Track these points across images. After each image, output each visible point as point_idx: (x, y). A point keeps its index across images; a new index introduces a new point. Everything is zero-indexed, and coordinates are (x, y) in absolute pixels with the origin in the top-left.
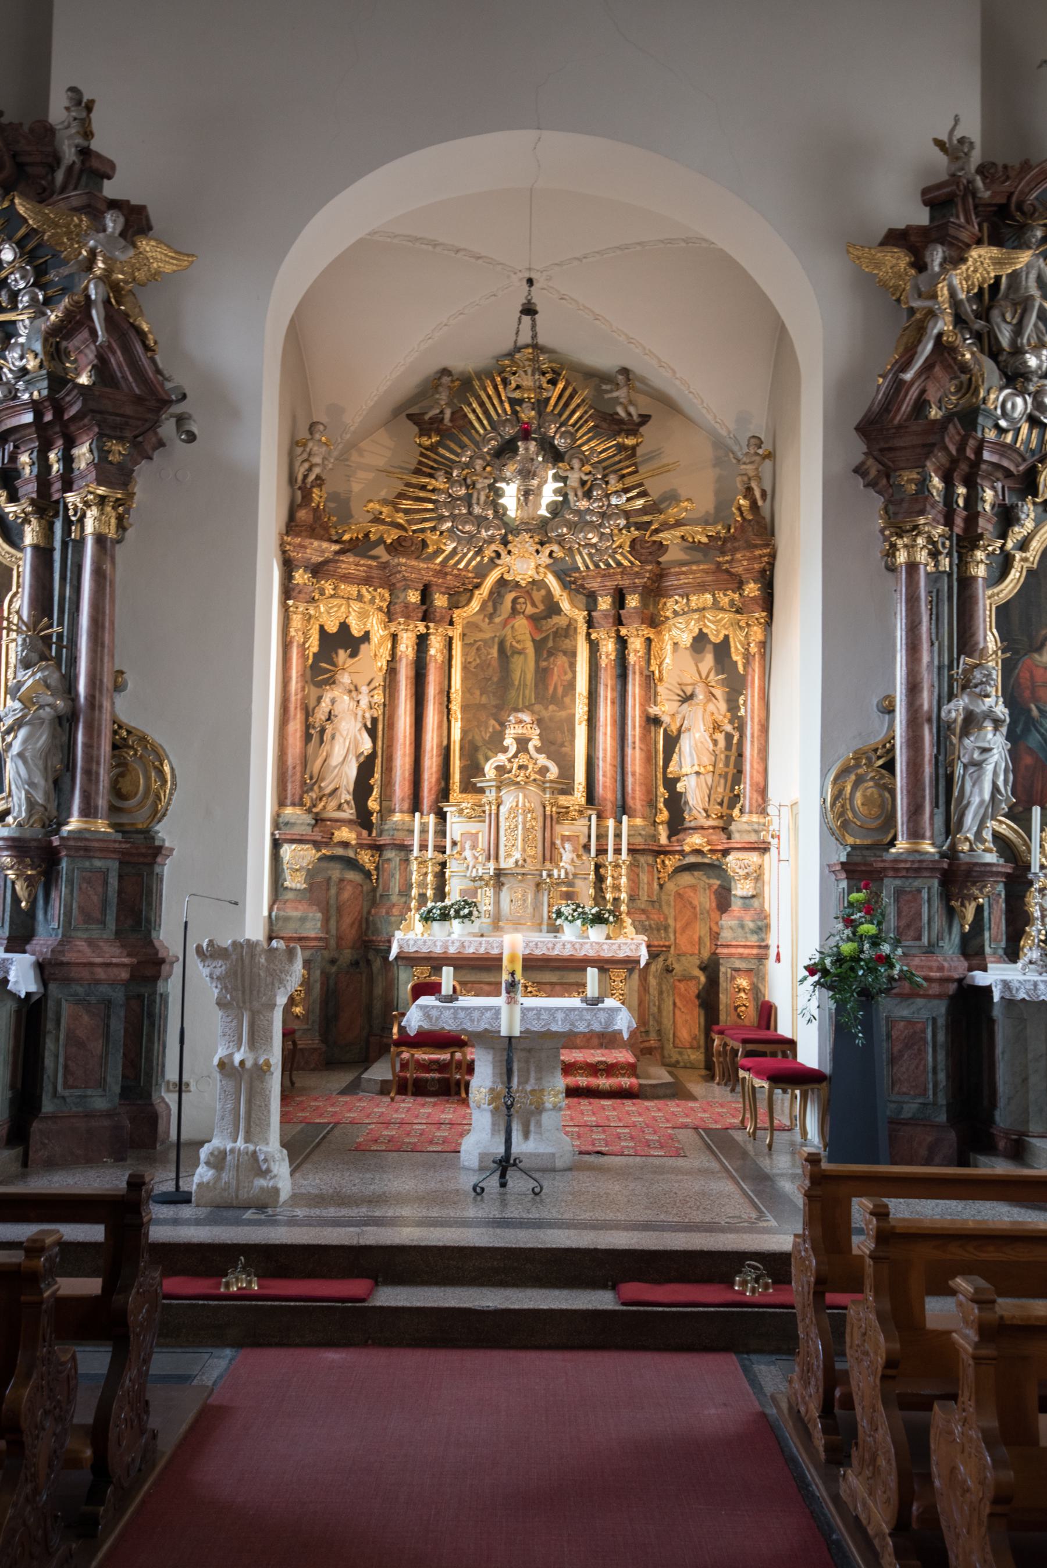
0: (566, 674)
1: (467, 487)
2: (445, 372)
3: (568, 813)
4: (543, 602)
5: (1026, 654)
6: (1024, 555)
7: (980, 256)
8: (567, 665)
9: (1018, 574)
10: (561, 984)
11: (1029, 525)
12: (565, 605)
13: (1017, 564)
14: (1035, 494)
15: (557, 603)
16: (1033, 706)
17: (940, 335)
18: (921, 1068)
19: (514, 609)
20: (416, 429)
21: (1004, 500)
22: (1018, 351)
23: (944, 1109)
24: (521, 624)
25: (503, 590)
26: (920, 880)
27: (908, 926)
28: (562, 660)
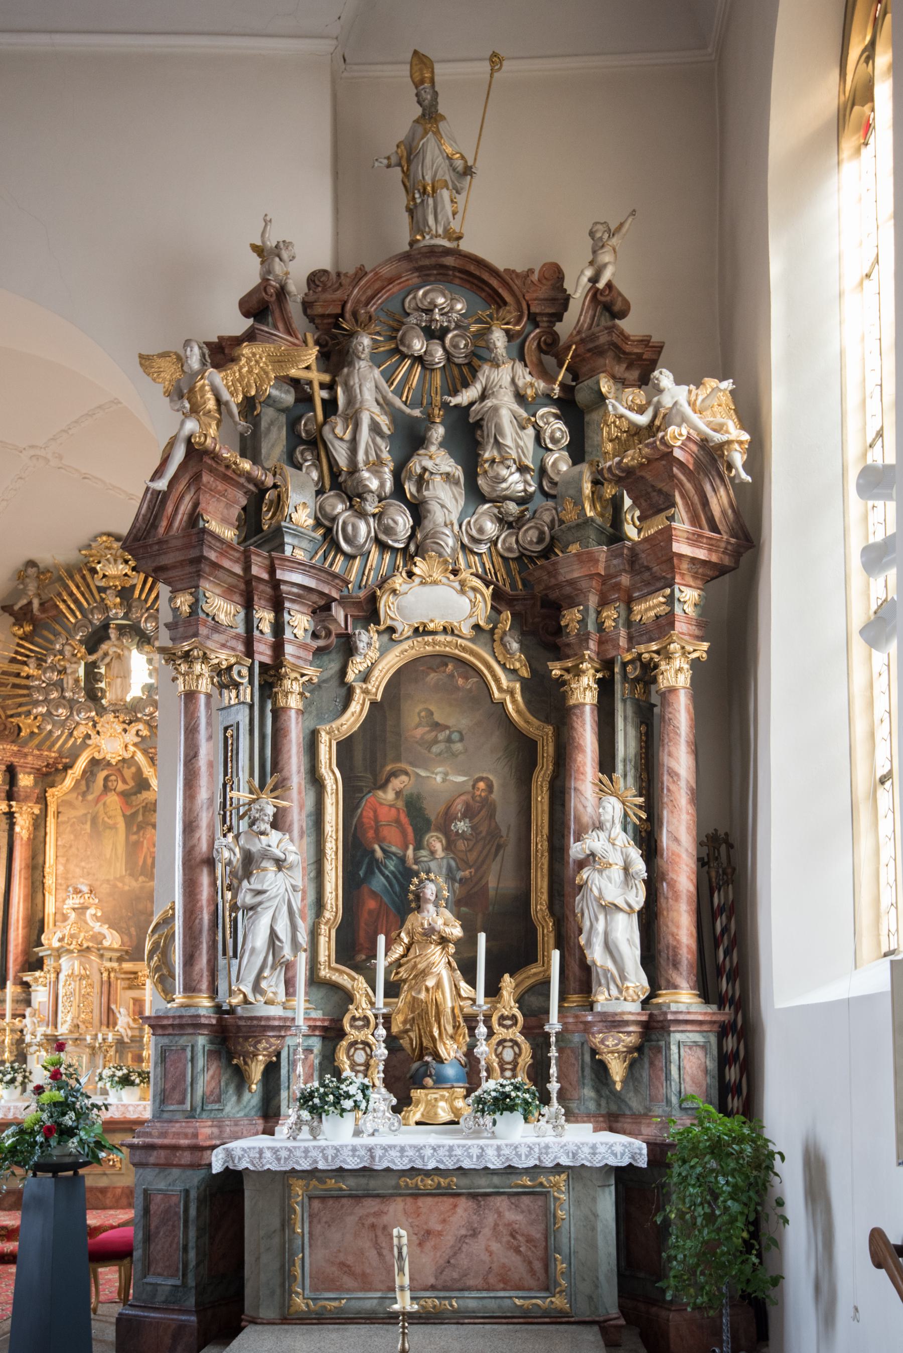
1: (60, 672)
2: (31, 563)
4: (133, 779)
5: (369, 792)
7: (254, 355)
11: (373, 654)
13: (358, 695)
14: (377, 623)
16: (377, 847)
18: (174, 1246)
19: (105, 786)
20: (12, 620)
21: (346, 628)
22: (354, 469)
23: (193, 1291)
24: (113, 799)
25: (95, 769)
26: (185, 1038)
27: (174, 1088)
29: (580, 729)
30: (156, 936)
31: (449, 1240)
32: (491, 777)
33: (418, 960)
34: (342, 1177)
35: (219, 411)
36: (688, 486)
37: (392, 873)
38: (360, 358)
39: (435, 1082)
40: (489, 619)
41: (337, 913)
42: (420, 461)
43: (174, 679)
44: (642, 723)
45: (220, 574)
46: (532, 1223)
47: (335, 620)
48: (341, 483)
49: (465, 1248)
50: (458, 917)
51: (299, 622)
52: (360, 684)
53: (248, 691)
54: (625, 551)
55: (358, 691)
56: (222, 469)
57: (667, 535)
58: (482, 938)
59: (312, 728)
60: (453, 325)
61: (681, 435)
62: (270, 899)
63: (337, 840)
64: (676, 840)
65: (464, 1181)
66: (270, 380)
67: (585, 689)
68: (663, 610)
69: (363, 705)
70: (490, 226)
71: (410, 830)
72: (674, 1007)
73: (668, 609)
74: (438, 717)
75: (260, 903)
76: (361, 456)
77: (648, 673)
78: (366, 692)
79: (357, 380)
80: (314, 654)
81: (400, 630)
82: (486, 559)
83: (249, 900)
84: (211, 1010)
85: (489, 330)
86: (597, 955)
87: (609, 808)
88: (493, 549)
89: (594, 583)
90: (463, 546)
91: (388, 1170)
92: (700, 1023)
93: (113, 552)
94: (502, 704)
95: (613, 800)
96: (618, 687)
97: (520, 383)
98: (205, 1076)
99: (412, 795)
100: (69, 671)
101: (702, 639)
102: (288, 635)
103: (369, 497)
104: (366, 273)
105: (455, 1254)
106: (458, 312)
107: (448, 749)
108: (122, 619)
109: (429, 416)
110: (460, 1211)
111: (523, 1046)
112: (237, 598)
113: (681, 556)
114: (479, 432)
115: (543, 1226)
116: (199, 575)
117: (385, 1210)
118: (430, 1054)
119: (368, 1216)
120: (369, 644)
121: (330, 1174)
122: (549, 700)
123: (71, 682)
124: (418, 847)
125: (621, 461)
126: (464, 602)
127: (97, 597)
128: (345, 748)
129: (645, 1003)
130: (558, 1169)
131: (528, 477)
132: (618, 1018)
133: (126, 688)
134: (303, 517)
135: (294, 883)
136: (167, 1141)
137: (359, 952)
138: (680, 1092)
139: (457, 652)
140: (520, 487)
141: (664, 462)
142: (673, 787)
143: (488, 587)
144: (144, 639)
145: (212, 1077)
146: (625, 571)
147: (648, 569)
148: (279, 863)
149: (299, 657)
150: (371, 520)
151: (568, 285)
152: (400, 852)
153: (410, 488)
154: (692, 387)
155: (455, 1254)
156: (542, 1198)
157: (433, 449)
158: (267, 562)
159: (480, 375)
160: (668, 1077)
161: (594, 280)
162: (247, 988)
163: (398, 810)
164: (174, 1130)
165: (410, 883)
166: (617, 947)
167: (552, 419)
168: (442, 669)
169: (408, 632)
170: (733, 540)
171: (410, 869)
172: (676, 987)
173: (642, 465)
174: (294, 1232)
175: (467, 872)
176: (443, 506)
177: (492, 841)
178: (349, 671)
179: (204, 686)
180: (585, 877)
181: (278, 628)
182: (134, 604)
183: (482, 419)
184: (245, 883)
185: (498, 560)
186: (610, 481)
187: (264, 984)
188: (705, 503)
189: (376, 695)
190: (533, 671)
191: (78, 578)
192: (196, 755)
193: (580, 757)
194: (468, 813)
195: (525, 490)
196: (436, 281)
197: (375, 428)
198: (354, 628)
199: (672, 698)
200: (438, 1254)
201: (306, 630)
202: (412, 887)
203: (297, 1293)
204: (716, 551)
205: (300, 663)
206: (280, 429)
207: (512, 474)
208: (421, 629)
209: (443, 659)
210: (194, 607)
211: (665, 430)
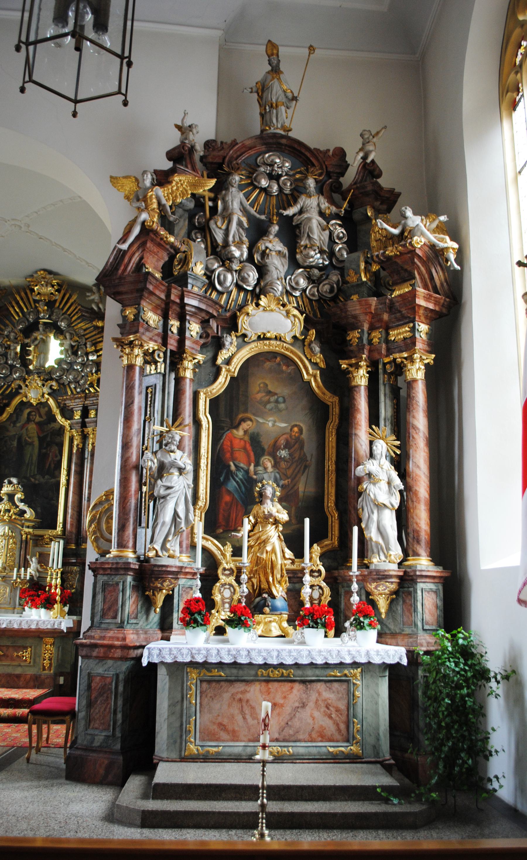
0: (56, 456)
1: (6, 348)
3: (42, 540)
4: (46, 415)
5: (228, 430)
6: (228, 367)
7: (180, 181)
8: (57, 452)
9: (224, 380)
10: (12, 646)
11: (233, 349)
12: (59, 417)
14: (236, 331)
15: (54, 415)
16: (231, 464)
17: (143, 223)
18: (107, 710)
22: (226, 244)
23: (119, 740)
24: (32, 426)
26: (118, 576)
27: (109, 609)
28: (55, 449)
29: (359, 400)
30: (94, 512)
31: (288, 709)
32: (301, 425)
33: (261, 534)
34: (222, 668)
35: (159, 209)
36: (423, 269)
37: (241, 480)
38: (233, 186)
39: (271, 610)
40: (302, 334)
41: (206, 503)
42: (265, 244)
43: (121, 357)
44: (394, 398)
45: (153, 298)
46: (339, 699)
47: (211, 328)
48: (219, 252)
49: (298, 715)
50: (284, 508)
51: (194, 328)
52: (225, 366)
53: (163, 366)
54: (387, 301)
55: (224, 370)
56: (158, 240)
57: (413, 294)
58: (307, 521)
59: (195, 390)
60: (284, 174)
61: (421, 242)
62: (174, 492)
63: (207, 458)
64: (418, 467)
65: (299, 672)
66: (188, 194)
67: (361, 377)
68: (408, 335)
69: (226, 378)
70: (303, 124)
71: (252, 454)
72: (419, 568)
73: (411, 335)
74: (270, 388)
75: (169, 495)
76: (231, 239)
77: (399, 369)
78: (228, 371)
79: (230, 198)
80: (201, 347)
81: (249, 336)
82: (299, 299)
83: (162, 492)
84: (135, 560)
85: (306, 178)
86: (373, 534)
87: (379, 447)
88: (303, 294)
89: (368, 318)
90: (287, 292)
91: (250, 664)
92: (434, 577)
93: (46, 280)
94: (309, 383)
95: (381, 441)
96: (381, 377)
97: (323, 206)
98: (130, 603)
99: (254, 433)
100: (12, 348)
101: (430, 352)
102: (187, 334)
103: (235, 261)
104: (237, 144)
105: (291, 719)
106: (287, 167)
107: (277, 407)
108: (47, 319)
109: (270, 219)
110: (295, 691)
111: (325, 589)
112: (159, 312)
113: (420, 306)
114: (298, 230)
115: (346, 701)
116: (141, 297)
117: (248, 690)
118: (266, 593)
119: (237, 693)
120: (231, 343)
121: (214, 666)
122: (338, 382)
123: (13, 354)
124: (257, 464)
125: (385, 252)
126: (288, 323)
127: (33, 306)
128: (215, 404)
129: (400, 564)
130: (355, 665)
131: (325, 257)
132: (386, 573)
133: (46, 359)
134: (199, 269)
135: (189, 483)
136: (105, 642)
137: (219, 527)
138: (423, 620)
139: (283, 350)
140: (321, 261)
141: (409, 255)
142: (415, 436)
143: (302, 315)
144: (59, 332)
145: (134, 603)
146: (386, 312)
147: (400, 312)
148: (181, 470)
149: (193, 349)
150: (234, 273)
151: (349, 159)
152: (245, 467)
153: (257, 257)
154: (423, 217)
155: (291, 719)
156: (346, 684)
157: (271, 237)
158: (180, 293)
159: (300, 200)
160: (415, 610)
161: (365, 158)
162: (158, 547)
163: (245, 441)
164: (109, 635)
165: (257, 486)
166: (385, 530)
167: (337, 227)
168: (274, 360)
169: (254, 338)
170: (448, 300)
171: (251, 478)
172: (418, 555)
173: (396, 255)
174: (190, 703)
175: (286, 481)
176: (276, 269)
177: (299, 463)
178: (219, 358)
179: (139, 361)
180: (365, 487)
181: (182, 331)
182: (56, 310)
183: (301, 224)
184: (159, 482)
185: (306, 301)
186: (375, 262)
187: (168, 545)
188: (432, 278)
189: (234, 372)
190: (327, 364)
191: (23, 294)
192: (133, 402)
193: (358, 416)
194: (287, 446)
195: (323, 263)
196: (277, 151)
197: (240, 224)
198: (222, 333)
199: (415, 385)
200: (281, 719)
201: (197, 333)
202: (257, 489)
203: (191, 742)
204: (438, 305)
205: (194, 352)
206: (185, 220)
207: (316, 254)
208: (262, 336)
209: (273, 355)
210: (137, 316)
211: (411, 238)
